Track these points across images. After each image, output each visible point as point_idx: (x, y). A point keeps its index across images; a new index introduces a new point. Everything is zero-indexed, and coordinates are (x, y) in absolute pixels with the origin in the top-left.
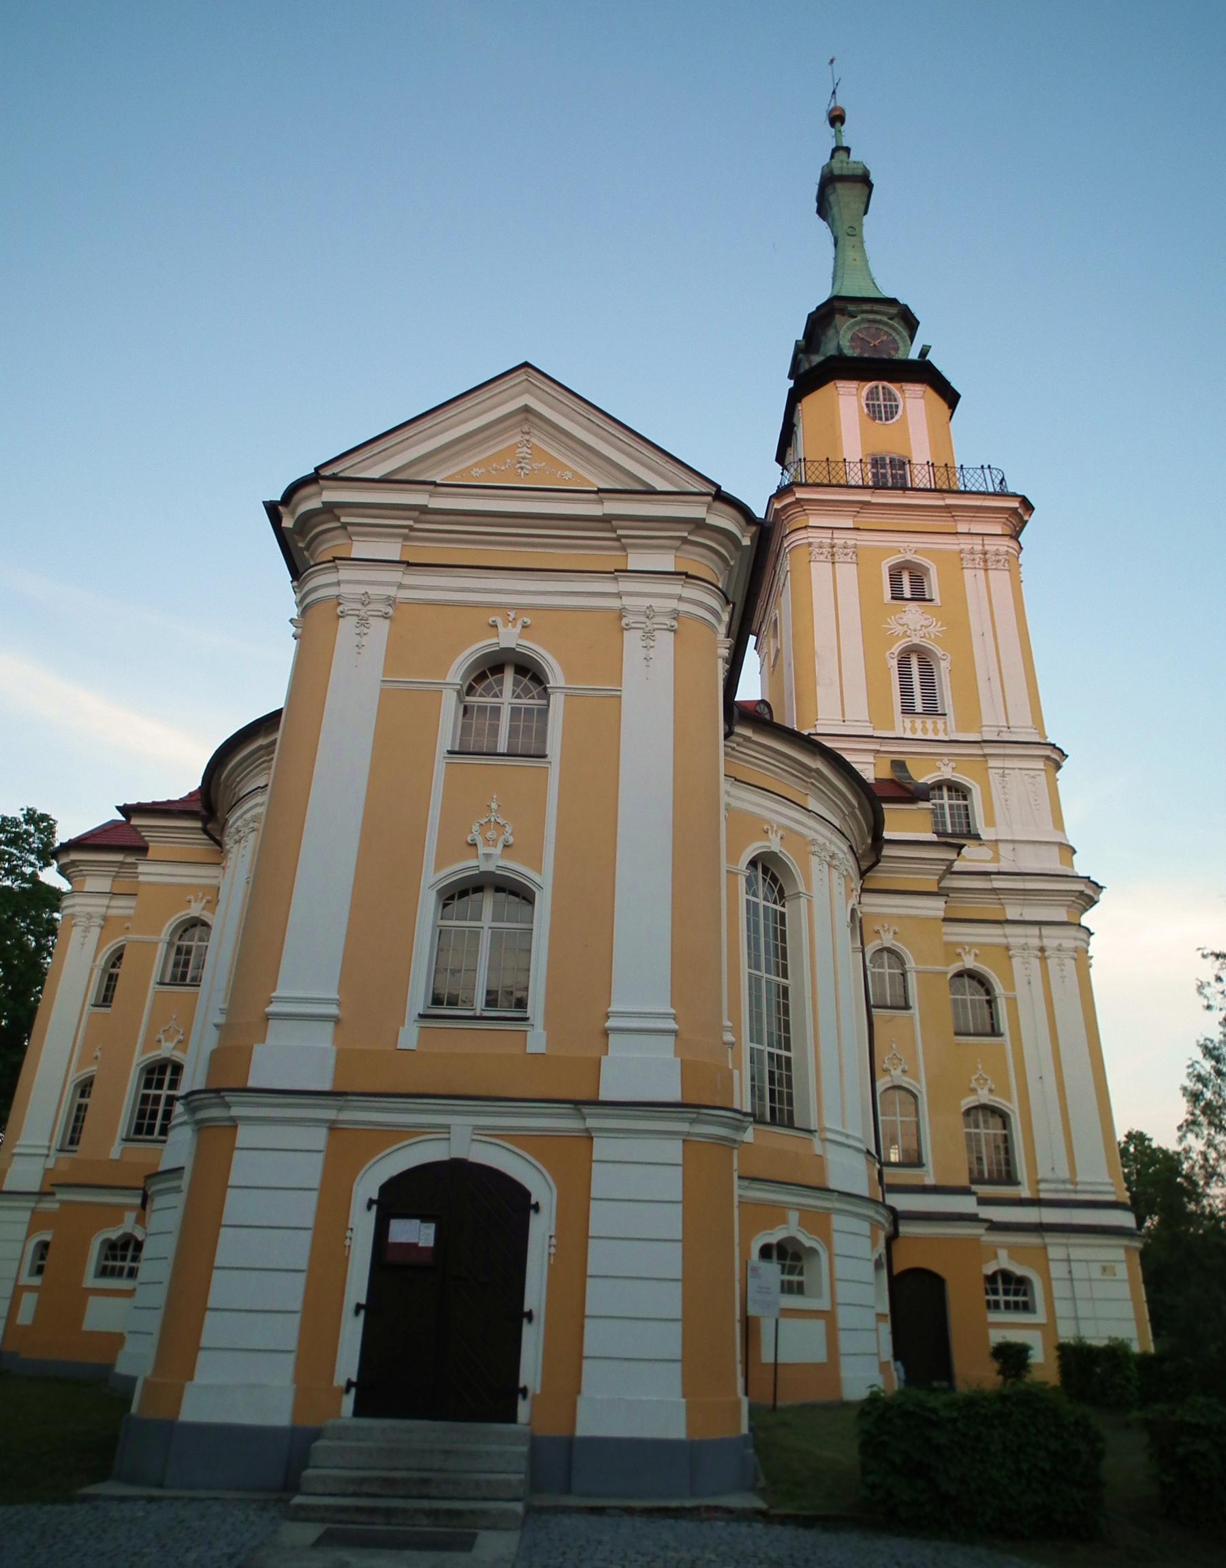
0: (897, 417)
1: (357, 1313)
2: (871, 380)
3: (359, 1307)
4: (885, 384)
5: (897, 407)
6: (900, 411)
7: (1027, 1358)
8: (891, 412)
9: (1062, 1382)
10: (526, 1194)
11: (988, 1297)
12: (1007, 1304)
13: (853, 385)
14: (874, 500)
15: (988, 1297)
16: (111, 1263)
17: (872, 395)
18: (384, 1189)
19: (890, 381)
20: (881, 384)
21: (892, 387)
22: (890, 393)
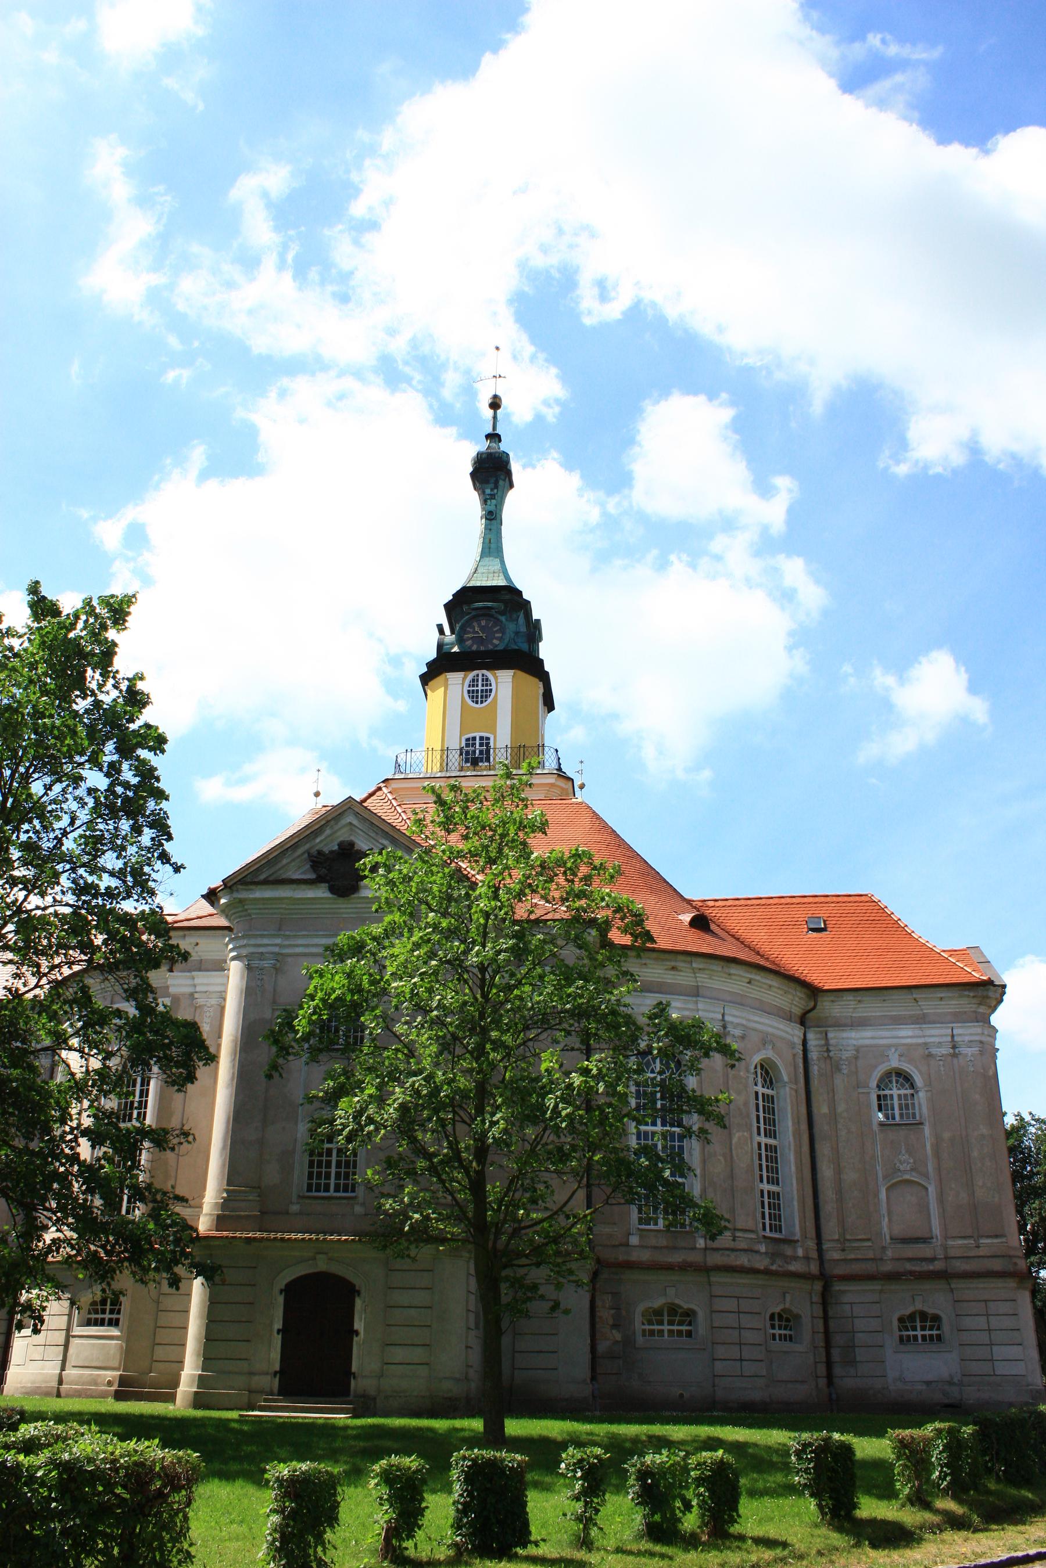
0: (489, 700)
1: (278, 1333)
3: (279, 1331)
4: (485, 672)
5: (491, 690)
6: (493, 694)
7: (970, 681)
8: (486, 694)
9: (521, 1504)
10: (353, 1286)
11: (644, 1327)
12: (924, 1337)
13: (460, 675)
15: (644, 1327)
16: (93, 1316)
17: (474, 681)
18: (286, 1285)
19: (488, 669)
20: (480, 672)
21: (488, 674)
22: (487, 680)
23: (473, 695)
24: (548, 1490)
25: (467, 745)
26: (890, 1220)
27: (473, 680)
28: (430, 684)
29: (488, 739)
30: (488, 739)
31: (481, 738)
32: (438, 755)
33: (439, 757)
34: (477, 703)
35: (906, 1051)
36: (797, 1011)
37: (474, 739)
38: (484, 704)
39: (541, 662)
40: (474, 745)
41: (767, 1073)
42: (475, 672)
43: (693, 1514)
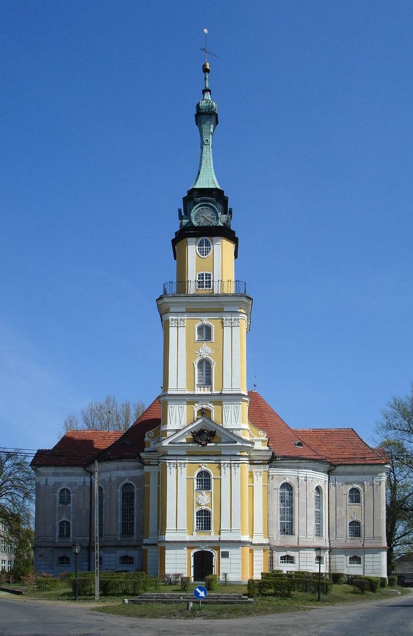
0: (209, 254)
2: (203, 236)
4: (206, 238)
5: (210, 249)
13: (195, 239)
14: (190, 301)
20: (204, 238)
23: (202, 252)
24: (122, 557)
25: (199, 278)
26: (117, 521)
27: (201, 242)
28: (178, 244)
29: (210, 275)
30: (210, 275)
31: (206, 275)
32: (233, 284)
33: (194, 285)
34: (203, 255)
35: (71, 484)
36: (327, 470)
37: (203, 275)
38: (207, 256)
39: (234, 233)
40: (203, 278)
41: (318, 489)
42: (202, 238)
43: (261, 447)
